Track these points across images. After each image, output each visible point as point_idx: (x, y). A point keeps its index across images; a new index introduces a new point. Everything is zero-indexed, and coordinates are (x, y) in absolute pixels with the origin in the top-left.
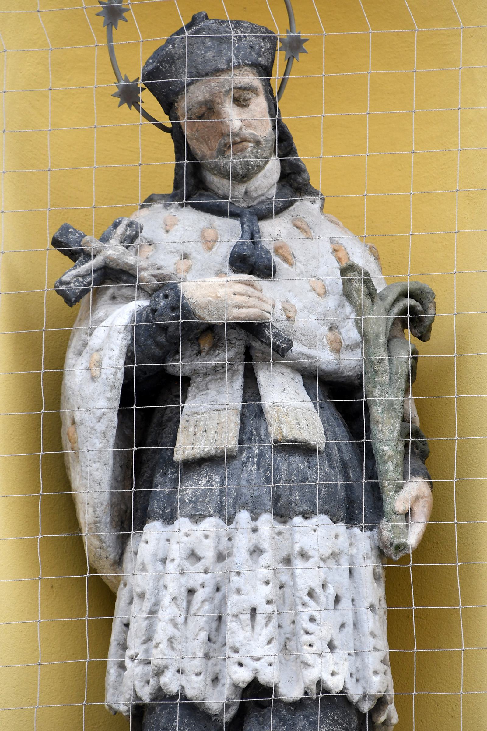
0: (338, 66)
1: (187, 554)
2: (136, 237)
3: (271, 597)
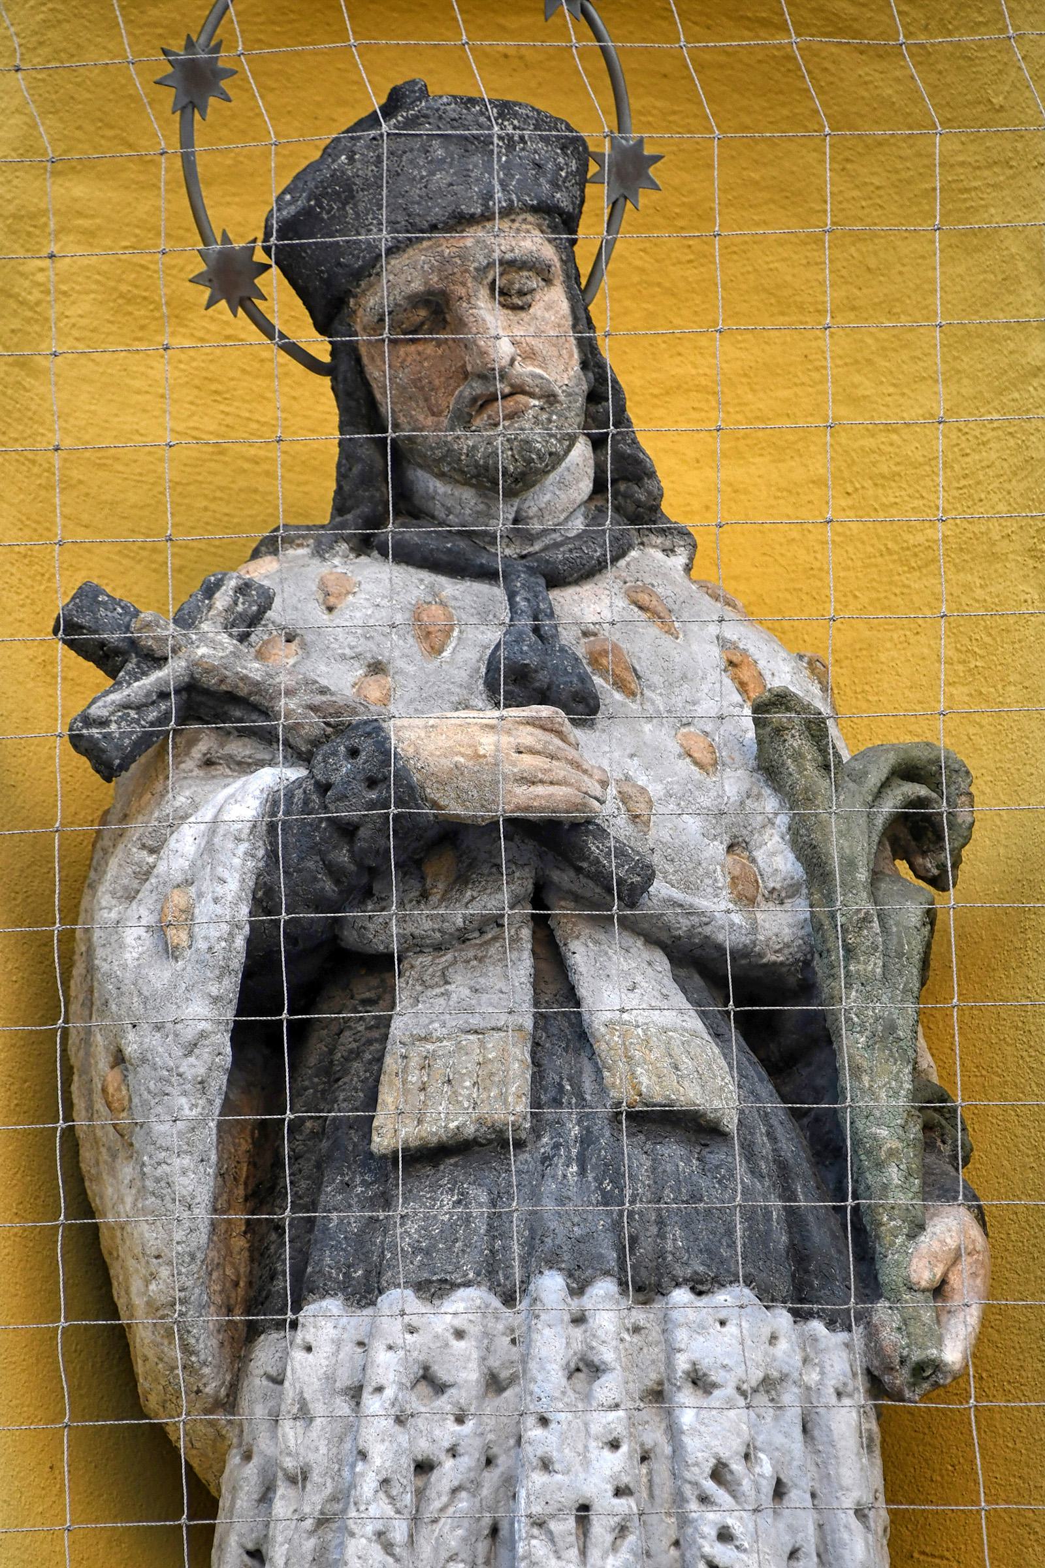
0: (689, 246)
1: (412, 1376)
2: (254, 620)
3: (625, 1479)
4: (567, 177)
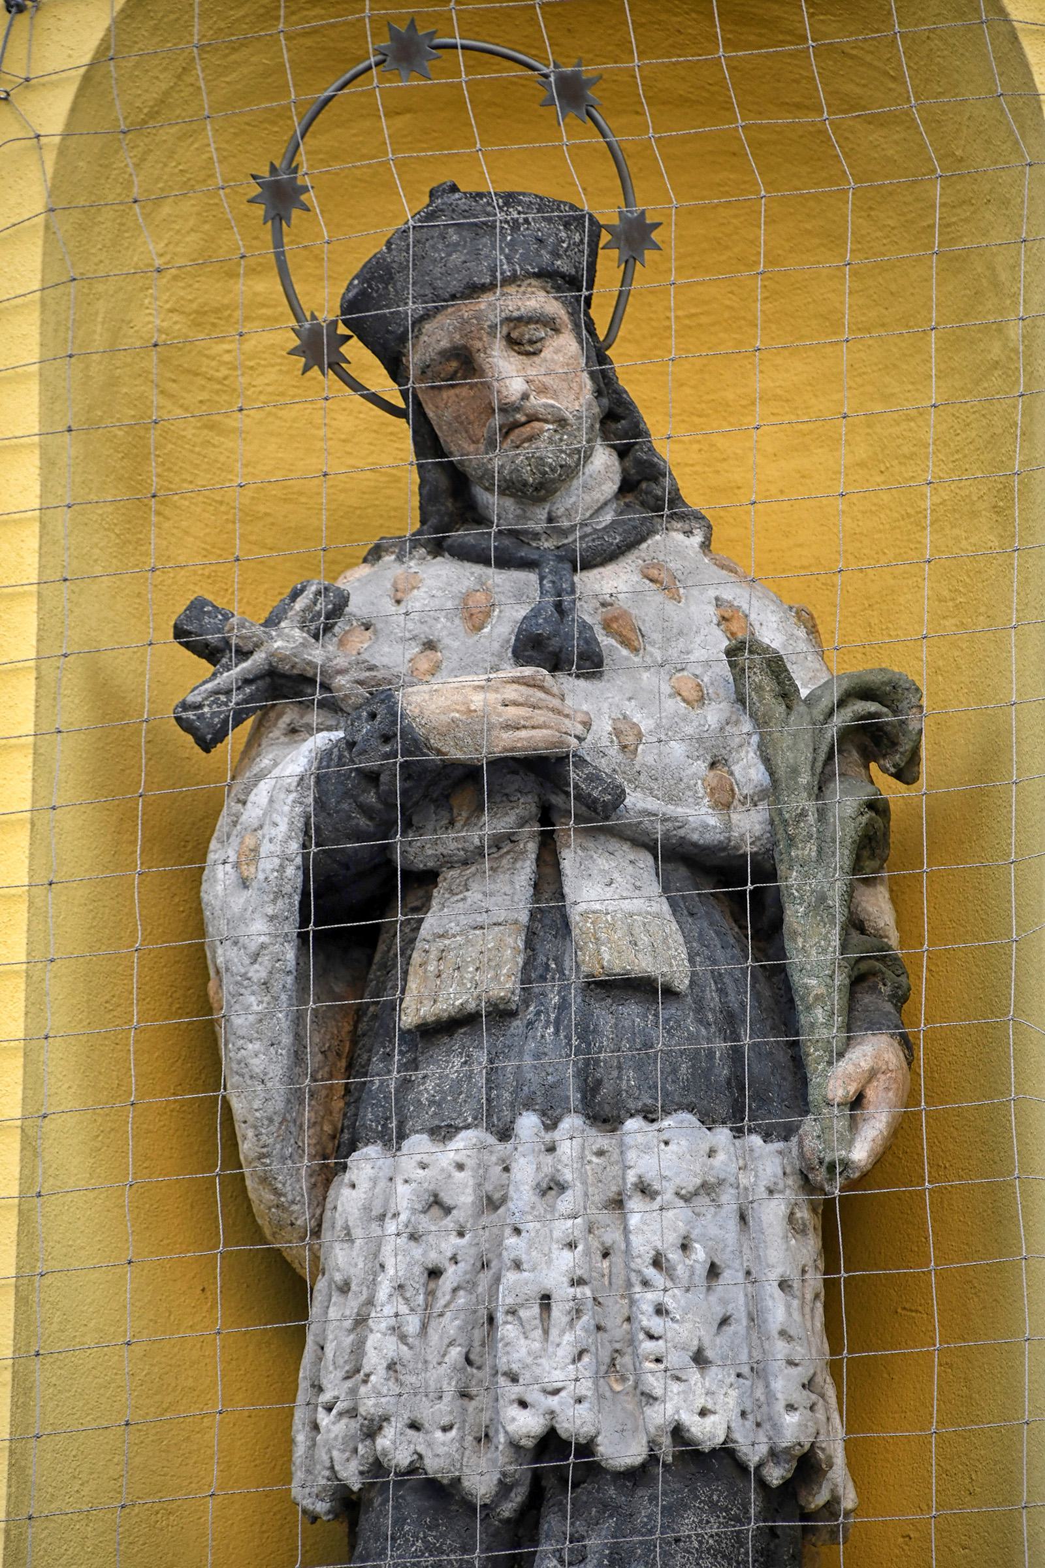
4: (568, 247)
